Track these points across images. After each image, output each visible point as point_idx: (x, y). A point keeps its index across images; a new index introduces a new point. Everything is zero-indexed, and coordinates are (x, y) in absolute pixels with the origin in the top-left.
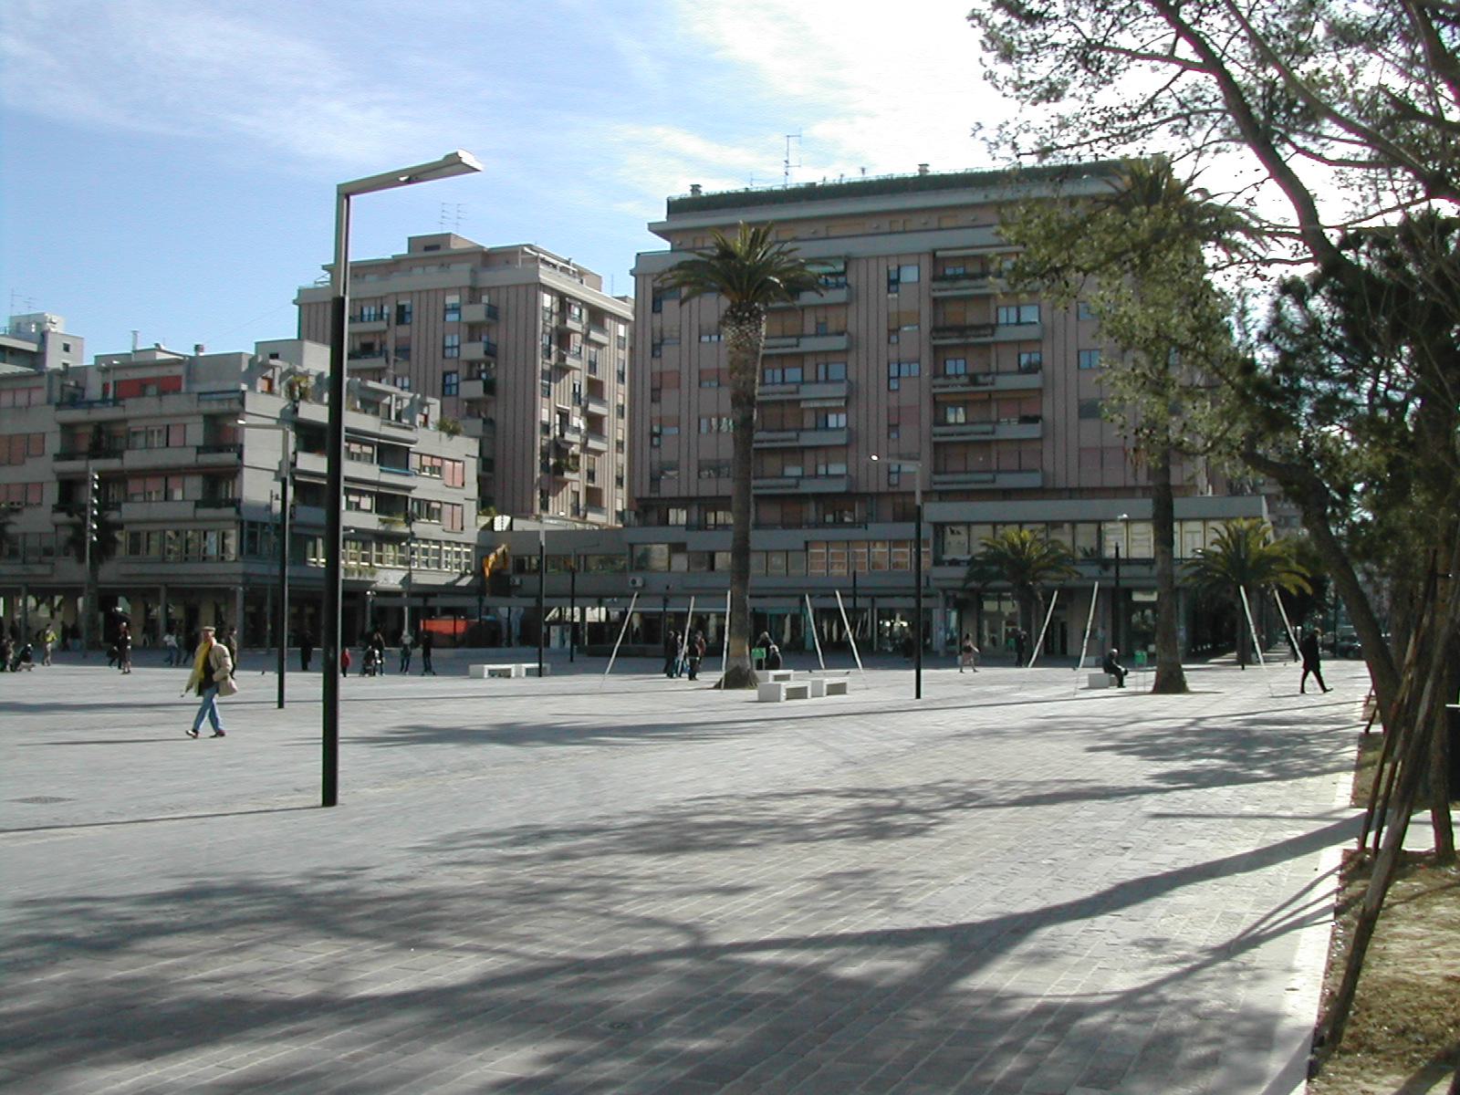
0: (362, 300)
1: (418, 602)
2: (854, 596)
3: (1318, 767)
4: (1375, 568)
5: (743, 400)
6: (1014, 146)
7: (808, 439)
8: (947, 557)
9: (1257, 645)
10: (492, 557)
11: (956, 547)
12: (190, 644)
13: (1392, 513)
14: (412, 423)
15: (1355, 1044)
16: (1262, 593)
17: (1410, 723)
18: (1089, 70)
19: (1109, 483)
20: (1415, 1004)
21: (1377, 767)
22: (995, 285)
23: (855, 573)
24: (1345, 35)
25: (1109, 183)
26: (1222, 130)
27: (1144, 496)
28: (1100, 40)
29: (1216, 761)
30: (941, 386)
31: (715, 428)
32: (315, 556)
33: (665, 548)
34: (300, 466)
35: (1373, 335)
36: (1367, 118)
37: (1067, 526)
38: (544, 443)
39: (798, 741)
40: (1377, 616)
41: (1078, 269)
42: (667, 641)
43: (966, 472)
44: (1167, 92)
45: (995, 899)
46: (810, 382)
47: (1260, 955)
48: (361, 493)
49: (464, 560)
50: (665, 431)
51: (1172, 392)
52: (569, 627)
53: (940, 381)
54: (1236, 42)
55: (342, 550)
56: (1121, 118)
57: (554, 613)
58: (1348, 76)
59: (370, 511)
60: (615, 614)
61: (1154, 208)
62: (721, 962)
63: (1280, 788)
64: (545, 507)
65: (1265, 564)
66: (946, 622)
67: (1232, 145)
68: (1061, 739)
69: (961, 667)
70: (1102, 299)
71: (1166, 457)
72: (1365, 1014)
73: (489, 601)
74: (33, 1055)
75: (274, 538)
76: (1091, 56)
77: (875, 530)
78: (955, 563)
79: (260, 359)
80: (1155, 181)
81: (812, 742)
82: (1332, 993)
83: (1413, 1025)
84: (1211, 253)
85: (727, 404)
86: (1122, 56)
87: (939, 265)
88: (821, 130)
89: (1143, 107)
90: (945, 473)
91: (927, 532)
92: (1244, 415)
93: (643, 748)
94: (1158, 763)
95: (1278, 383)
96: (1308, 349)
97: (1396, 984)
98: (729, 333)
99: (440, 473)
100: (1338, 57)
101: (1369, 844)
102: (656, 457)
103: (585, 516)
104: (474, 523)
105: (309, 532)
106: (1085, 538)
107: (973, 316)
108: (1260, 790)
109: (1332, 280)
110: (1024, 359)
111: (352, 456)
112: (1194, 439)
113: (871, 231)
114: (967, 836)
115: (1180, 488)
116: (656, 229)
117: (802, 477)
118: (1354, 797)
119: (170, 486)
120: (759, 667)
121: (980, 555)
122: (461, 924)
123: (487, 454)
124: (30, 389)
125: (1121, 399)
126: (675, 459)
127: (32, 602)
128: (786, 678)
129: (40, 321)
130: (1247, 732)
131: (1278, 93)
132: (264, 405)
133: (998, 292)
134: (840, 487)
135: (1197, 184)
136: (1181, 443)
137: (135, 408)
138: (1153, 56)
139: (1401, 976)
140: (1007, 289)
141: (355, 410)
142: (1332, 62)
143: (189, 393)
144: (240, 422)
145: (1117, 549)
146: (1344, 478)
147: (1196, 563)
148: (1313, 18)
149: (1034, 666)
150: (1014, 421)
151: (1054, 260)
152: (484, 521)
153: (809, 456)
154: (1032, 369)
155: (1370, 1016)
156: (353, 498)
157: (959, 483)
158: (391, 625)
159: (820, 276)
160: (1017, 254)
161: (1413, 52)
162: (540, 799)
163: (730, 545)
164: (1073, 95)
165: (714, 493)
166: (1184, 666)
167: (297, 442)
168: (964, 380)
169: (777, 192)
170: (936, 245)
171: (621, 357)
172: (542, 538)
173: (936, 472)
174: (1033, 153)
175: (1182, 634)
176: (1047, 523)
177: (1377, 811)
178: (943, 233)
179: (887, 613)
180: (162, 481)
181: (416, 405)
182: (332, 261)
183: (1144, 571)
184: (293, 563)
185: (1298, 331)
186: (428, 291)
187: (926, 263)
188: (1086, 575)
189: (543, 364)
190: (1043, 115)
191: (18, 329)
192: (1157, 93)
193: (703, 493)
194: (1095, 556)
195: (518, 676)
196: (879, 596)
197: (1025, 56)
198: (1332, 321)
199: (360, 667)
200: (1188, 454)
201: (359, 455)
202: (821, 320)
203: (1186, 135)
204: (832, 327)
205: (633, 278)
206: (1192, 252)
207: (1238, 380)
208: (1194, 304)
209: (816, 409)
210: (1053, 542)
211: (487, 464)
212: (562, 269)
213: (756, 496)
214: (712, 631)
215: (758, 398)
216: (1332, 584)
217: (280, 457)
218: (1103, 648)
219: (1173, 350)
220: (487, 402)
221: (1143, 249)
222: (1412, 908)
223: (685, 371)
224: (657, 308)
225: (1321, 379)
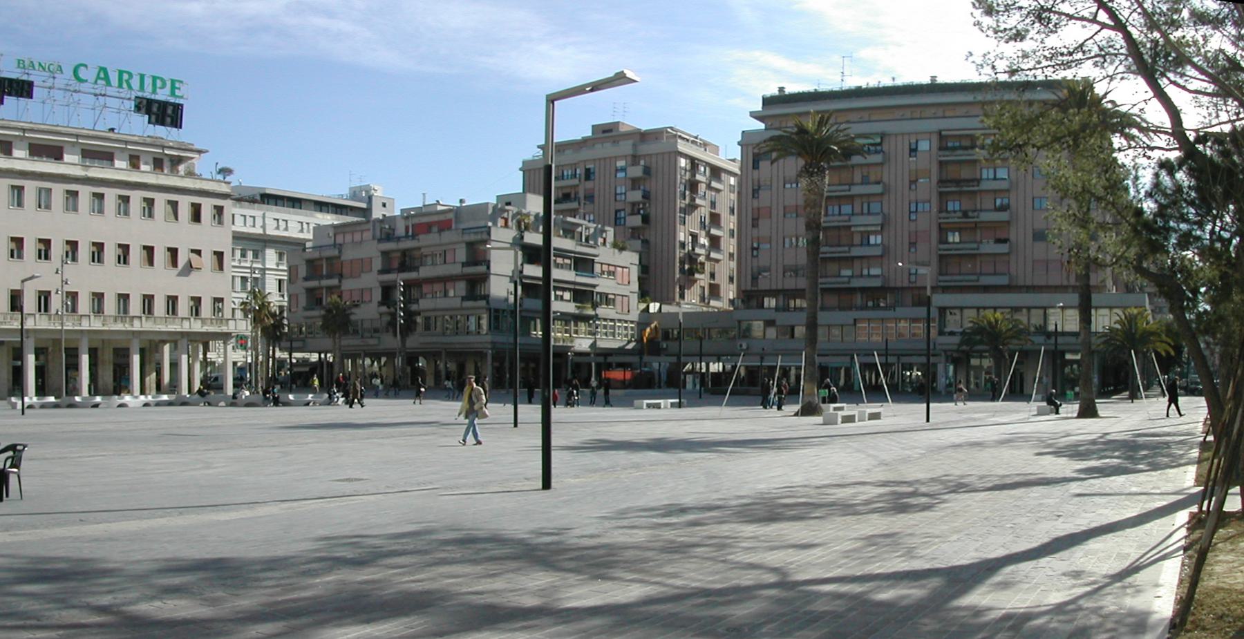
0: (563, 166)
1: (601, 359)
2: (886, 355)
3: (1176, 463)
4: (1211, 340)
5: (813, 226)
6: (993, 67)
7: (856, 252)
8: (947, 330)
9: (1141, 387)
10: (648, 330)
11: (953, 323)
12: (460, 386)
13: (1222, 306)
14: (596, 243)
15: (1194, 626)
16: (1145, 354)
17: (1229, 435)
18: (1042, 24)
19: (1051, 283)
20: (1228, 600)
21: (1210, 461)
22: (980, 154)
23: (887, 340)
24: (1200, 18)
25: (1054, 93)
26: (1125, 66)
27: (1073, 292)
28: (1049, 7)
29: (1115, 460)
30: (944, 218)
31: (794, 244)
32: (535, 330)
33: (761, 323)
34: (526, 272)
35: (1213, 197)
36: (1212, 67)
37: (1024, 311)
38: (682, 255)
39: (849, 450)
40: (1212, 369)
41: (1034, 146)
42: (763, 384)
43: (960, 274)
44: (1091, 41)
45: (976, 550)
46: (858, 214)
47: (1140, 578)
48: (564, 289)
49: (630, 332)
50: (761, 246)
51: (1092, 226)
52: (699, 375)
53: (944, 215)
54: (1135, 15)
55: (552, 326)
56: (1062, 54)
57: (689, 367)
58: (1201, 42)
59: (569, 301)
60: (728, 367)
61: (1082, 110)
62: (799, 591)
63: (1153, 476)
64: (682, 296)
65: (1147, 336)
66: (946, 372)
67: (1131, 76)
68: (1019, 448)
69: (955, 401)
70: (1049, 165)
71: (1087, 267)
72: (1200, 608)
73: (646, 358)
74: (304, 620)
75: (510, 319)
76: (1044, 16)
77: (900, 311)
78: (952, 333)
79: (499, 206)
80: (1083, 94)
81: (858, 451)
82: (1181, 598)
83: (1227, 612)
84: (1117, 141)
85: (802, 228)
86: (1063, 17)
87: (943, 139)
88: (865, 53)
89: (1076, 48)
90: (946, 274)
91: (934, 313)
92: (1136, 242)
93: (746, 455)
94: (1080, 462)
95: (1157, 223)
96: (1175, 203)
97: (1218, 589)
98: (804, 183)
99: (614, 276)
100: (1196, 30)
101: (1205, 508)
102: (755, 264)
103: (709, 303)
104: (636, 307)
105: (531, 315)
106: (1036, 318)
107: (965, 173)
108: (1141, 477)
109: (1190, 162)
110: (998, 202)
111: (557, 266)
112: (1105, 256)
113: (898, 117)
114: (959, 511)
115: (1096, 287)
116: (754, 115)
117: (852, 277)
118: (1196, 481)
119: (447, 287)
120: (824, 402)
121: (968, 328)
122: (630, 565)
123: (644, 262)
124: (362, 231)
125: (1060, 229)
126: (768, 264)
127: (368, 361)
128: (841, 409)
129: (368, 189)
130: (1134, 441)
131: (1160, 48)
132: (502, 235)
133: (982, 158)
134: (877, 283)
135: (1109, 97)
136: (1097, 259)
137: (425, 240)
138: (1083, 19)
139: (1221, 585)
140: (988, 156)
141: (559, 236)
142: (1193, 33)
143: (456, 229)
144: (488, 246)
145: (1056, 325)
146: (1195, 284)
147: (1104, 335)
148: (1182, 6)
149: (1003, 401)
150: (992, 242)
151: (1018, 140)
152: (643, 306)
153: (857, 264)
154: (1003, 208)
155: (1203, 610)
156: (559, 293)
157: (955, 281)
158: (584, 374)
159: (864, 145)
160: (995, 135)
161: (1240, 32)
162: (681, 487)
163: (804, 321)
164: (1032, 39)
165: (793, 287)
166: (1096, 401)
167: (523, 257)
168: (959, 214)
169: (836, 92)
170: (942, 127)
171: (732, 198)
172: (681, 317)
173: (941, 274)
174: (1005, 72)
175: (1096, 380)
176: (1012, 308)
177: (1209, 488)
178: (946, 120)
179: (908, 367)
180: (442, 285)
181: (598, 231)
182: (543, 143)
183: (1072, 340)
184: (522, 335)
185: (1169, 192)
186: (605, 159)
187: (935, 138)
188: (1036, 342)
189: (680, 203)
190: (1012, 49)
191: (354, 195)
192: (1085, 41)
193: (786, 287)
194: (1042, 330)
195: (666, 407)
196: (903, 355)
197: (1001, 13)
198: (1189, 187)
199: (564, 401)
200: (1101, 265)
201: (562, 265)
202: (865, 174)
203: (1103, 68)
204: (872, 178)
205: (739, 147)
206: (1105, 139)
207: (1132, 220)
208: (1106, 172)
209: (861, 232)
210: (1016, 320)
211: (644, 269)
212: (693, 142)
213: (821, 289)
214: (793, 378)
215: (823, 225)
216: (1186, 349)
217: (512, 267)
218: (1047, 390)
219: (1093, 199)
220: (644, 229)
221: (1075, 136)
222: (1228, 544)
223: (774, 207)
224: (755, 166)
225: (1182, 222)
